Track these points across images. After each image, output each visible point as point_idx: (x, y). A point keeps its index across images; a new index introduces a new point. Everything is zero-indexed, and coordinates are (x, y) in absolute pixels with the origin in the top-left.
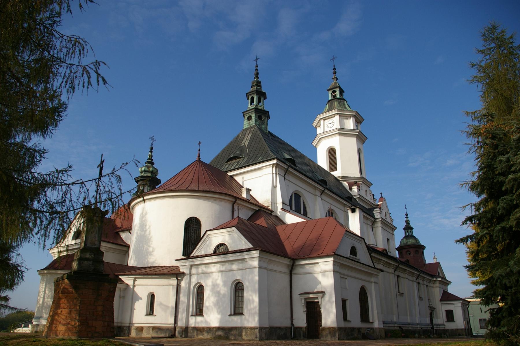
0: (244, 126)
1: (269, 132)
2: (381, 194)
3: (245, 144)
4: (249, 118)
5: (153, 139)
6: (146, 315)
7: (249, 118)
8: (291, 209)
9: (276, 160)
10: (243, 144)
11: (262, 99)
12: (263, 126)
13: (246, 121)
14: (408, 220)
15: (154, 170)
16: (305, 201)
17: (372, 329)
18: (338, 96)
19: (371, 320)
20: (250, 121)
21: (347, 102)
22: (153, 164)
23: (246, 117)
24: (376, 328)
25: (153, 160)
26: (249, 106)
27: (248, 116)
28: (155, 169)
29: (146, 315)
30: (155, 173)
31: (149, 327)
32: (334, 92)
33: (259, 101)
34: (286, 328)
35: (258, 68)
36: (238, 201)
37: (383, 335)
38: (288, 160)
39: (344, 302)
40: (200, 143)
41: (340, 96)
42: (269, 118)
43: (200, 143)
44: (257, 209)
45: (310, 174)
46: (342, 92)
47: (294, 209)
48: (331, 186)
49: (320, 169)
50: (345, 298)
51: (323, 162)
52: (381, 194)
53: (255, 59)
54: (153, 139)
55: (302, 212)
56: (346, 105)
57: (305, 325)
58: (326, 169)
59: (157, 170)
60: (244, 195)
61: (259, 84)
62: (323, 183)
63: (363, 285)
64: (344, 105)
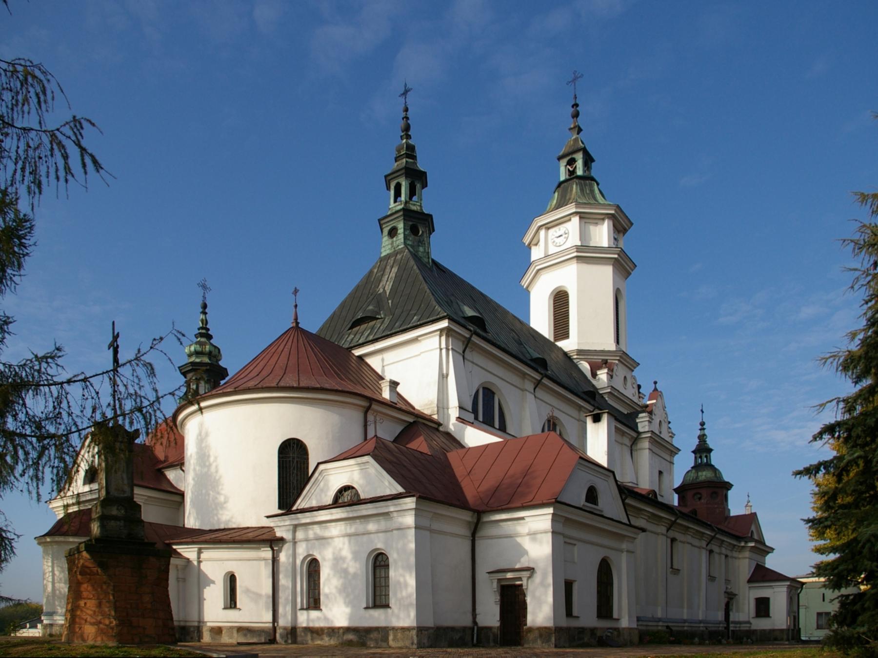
0: (383, 250)
1: (433, 261)
4: (393, 233)
5: (204, 287)
7: (393, 233)
8: (476, 418)
10: (381, 290)
11: (418, 186)
12: (421, 249)
13: (386, 240)
17: (617, 629)
19: (615, 616)
20: (395, 239)
21: (598, 184)
22: (209, 337)
24: (624, 629)
25: (208, 330)
26: (392, 205)
27: (389, 228)
28: (215, 347)
30: (215, 356)
31: (231, 628)
32: (572, 162)
34: (464, 629)
36: (375, 406)
37: (636, 639)
38: (471, 319)
40: (296, 291)
43: (296, 291)
45: (513, 348)
46: (588, 161)
54: (204, 287)
55: (497, 425)
57: (498, 624)
59: (219, 350)
61: (410, 152)
62: (540, 364)
63: (605, 557)
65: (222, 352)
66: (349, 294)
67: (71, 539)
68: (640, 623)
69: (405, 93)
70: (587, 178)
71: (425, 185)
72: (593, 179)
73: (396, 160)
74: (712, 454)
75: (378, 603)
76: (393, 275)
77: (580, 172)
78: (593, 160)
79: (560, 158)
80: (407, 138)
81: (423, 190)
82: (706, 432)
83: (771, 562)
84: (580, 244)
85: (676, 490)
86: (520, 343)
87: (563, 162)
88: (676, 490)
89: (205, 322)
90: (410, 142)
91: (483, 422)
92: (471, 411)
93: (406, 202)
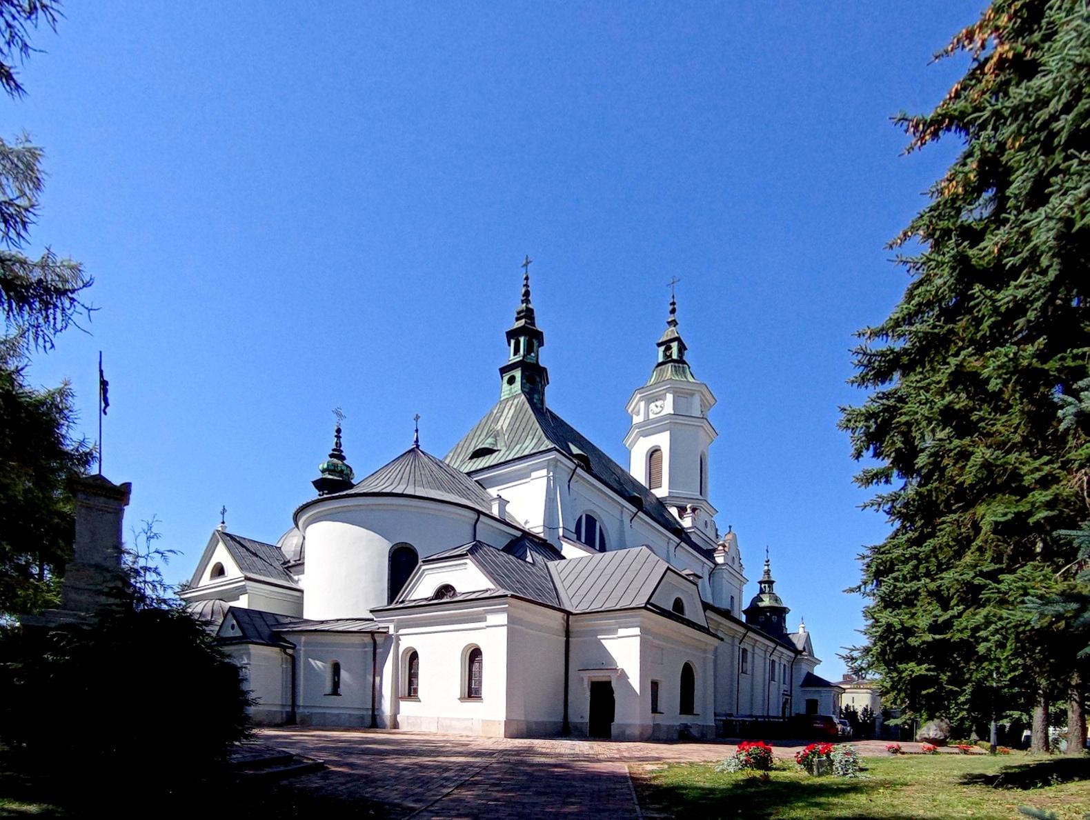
0: (503, 394)
1: (547, 409)
2: (730, 527)
3: (502, 428)
4: (511, 381)
5: (339, 415)
6: (420, 701)
7: (511, 381)
8: (579, 538)
9: (638, 629)
10: (499, 428)
11: (536, 343)
13: (505, 386)
14: (769, 570)
15: (344, 468)
16: (604, 532)
18: (675, 356)
20: (513, 386)
21: (689, 368)
22: (342, 458)
23: (506, 378)
25: (342, 451)
26: (512, 357)
27: (508, 377)
28: (348, 466)
29: (420, 701)
30: (347, 475)
32: (669, 348)
33: (529, 348)
35: (530, 283)
36: (482, 518)
37: (675, 736)
38: (577, 456)
39: (655, 685)
40: (417, 418)
41: (678, 356)
42: (548, 383)
43: (417, 418)
44: (519, 534)
45: (615, 485)
46: (682, 348)
47: (583, 540)
48: (648, 508)
49: (634, 482)
50: (656, 678)
51: (638, 471)
52: (730, 527)
53: (524, 262)
54: (339, 415)
55: (597, 547)
56: (688, 373)
58: (644, 484)
59: (351, 471)
60: (495, 511)
61: (528, 314)
62: (637, 502)
64: (684, 372)
65: (354, 471)
66: (613, 772)
67: (313, 664)
68: (717, 718)
69: (526, 265)
70: (681, 361)
71: (541, 344)
72: (684, 362)
73: (518, 319)
74: (774, 585)
75: (368, 639)
76: (510, 415)
77: (675, 356)
78: (686, 349)
79: (659, 345)
80: (527, 304)
81: (540, 349)
82: (770, 568)
83: (818, 671)
84: (672, 412)
85: (745, 612)
86: (621, 484)
87: (662, 348)
88: (745, 612)
89: (338, 444)
90: (530, 306)
91: (586, 543)
92: (574, 531)
93: (524, 356)
